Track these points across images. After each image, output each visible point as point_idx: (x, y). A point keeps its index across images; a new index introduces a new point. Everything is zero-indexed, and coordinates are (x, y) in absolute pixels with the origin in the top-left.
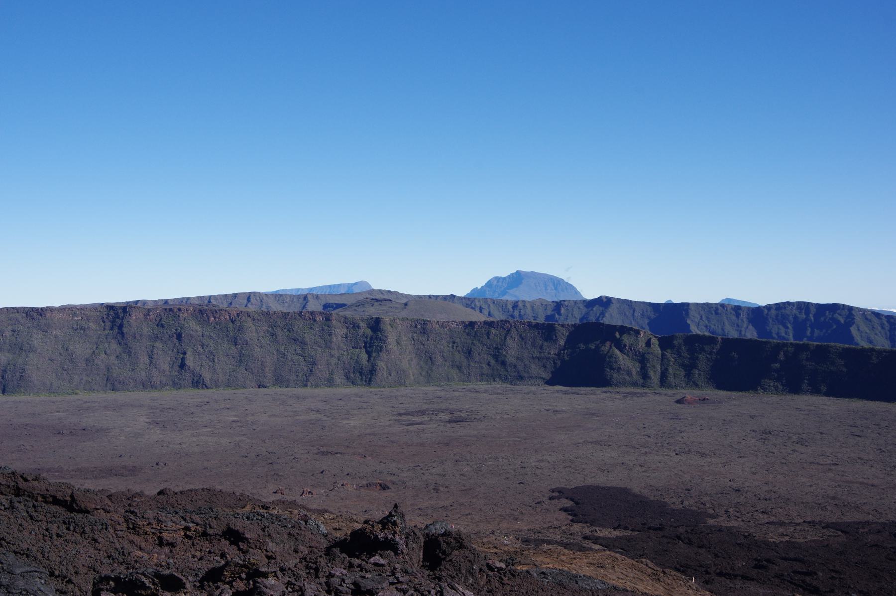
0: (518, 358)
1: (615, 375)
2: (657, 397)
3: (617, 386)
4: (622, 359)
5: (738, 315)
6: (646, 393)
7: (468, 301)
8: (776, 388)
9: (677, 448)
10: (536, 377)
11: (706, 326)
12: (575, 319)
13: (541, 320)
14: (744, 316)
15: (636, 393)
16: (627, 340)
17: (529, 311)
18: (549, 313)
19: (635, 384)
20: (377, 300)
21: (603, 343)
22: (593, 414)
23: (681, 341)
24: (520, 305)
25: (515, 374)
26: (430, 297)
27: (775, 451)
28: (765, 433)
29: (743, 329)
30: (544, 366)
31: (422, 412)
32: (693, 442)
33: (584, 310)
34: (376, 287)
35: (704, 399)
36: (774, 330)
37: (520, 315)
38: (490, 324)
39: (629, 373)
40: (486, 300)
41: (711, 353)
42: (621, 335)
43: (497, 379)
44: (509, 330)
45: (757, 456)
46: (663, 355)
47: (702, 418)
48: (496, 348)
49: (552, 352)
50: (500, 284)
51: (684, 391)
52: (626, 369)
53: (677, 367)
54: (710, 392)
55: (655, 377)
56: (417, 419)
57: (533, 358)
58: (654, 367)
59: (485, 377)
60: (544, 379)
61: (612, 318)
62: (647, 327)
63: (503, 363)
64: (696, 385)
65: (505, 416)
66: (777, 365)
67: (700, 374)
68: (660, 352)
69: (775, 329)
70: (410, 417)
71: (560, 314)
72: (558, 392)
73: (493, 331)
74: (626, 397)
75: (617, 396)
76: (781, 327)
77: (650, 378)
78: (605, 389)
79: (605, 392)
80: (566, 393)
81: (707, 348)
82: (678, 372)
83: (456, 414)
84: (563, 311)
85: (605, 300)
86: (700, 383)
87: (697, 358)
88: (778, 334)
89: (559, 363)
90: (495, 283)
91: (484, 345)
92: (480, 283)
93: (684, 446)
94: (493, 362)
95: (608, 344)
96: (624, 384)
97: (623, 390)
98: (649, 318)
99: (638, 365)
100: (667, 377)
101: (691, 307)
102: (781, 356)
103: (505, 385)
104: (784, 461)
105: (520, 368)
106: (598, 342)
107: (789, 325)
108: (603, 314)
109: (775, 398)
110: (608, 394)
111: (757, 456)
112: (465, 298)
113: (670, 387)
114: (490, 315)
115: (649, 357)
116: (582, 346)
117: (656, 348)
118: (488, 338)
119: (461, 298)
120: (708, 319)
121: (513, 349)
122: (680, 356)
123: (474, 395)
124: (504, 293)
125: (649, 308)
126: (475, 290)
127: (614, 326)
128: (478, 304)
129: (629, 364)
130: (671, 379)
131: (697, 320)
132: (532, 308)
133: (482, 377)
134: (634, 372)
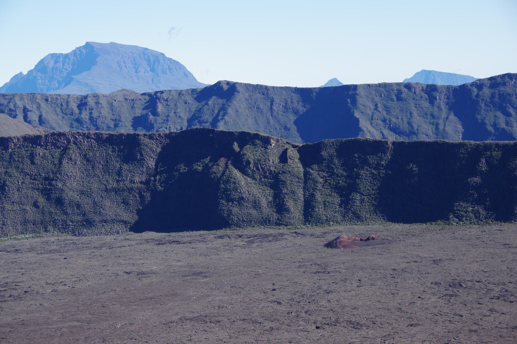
0: (82, 193)
1: (235, 210)
2: (299, 240)
3: (238, 226)
4: (245, 184)
5: (432, 100)
6: (282, 235)
8: (477, 215)
9: (319, 318)
10: (113, 221)
11: (384, 121)
12: (177, 124)
13: (126, 129)
14: (441, 100)
15: (267, 236)
16: (251, 153)
17: (105, 111)
18: (138, 112)
19: (265, 222)
21: (215, 160)
22: (199, 274)
23: (332, 151)
24: (91, 101)
25: (79, 218)
27: (464, 312)
28: (452, 285)
29: (441, 121)
30: (125, 203)
32: (343, 307)
33: (194, 105)
35: (368, 239)
36: (489, 120)
37: (91, 119)
38: (34, 140)
39: (256, 205)
40: (32, 97)
41: (377, 167)
42: (241, 147)
43: (50, 228)
44: (66, 149)
45: (436, 322)
46: (306, 174)
47: (362, 269)
48: (46, 179)
49: (137, 179)
50: (60, 65)
51: (340, 228)
52: (251, 199)
53: (328, 191)
54: (379, 227)
55: (295, 207)
57: (106, 190)
58: (293, 192)
59: (30, 226)
60: (125, 222)
61: (237, 119)
62: (294, 129)
63: (59, 202)
64: (358, 217)
65: (61, 288)
66: (477, 179)
67: (362, 201)
68: (302, 169)
69: (490, 117)
71: (155, 113)
72: (147, 241)
73: (40, 151)
74: (252, 242)
75: (239, 242)
76: (499, 114)
77: (288, 210)
78: (220, 232)
79: (221, 237)
80: (160, 243)
81: (372, 159)
82: (330, 199)
84: (160, 108)
85: (225, 87)
86: (363, 214)
87: (358, 175)
88: (494, 125)
89: (148, 196)
90: (51, 64)
91: (26, 174)
92: (26, 66)
93: (331, 314)
94: (42, 200)
95: (222, 161)
96: (249, 222)
97: (248, 231)
98: (296, 112)
99: (269, 191)
100: (313, 208)
101: (360, 91)
102: (483, 165)
103: (63, 237)
104: (474, 327)
105: (87, 208)
106: (207, 160)
107: (511, 111)
108: (223, 109)
109: (473, 230)
110: (226, 240)
111: (436, 322)
113: (319, 222)
114: (41, 121)
115: (287, 178)
116: (183, 168)
117: (295, 165)
118: (33, 163)
120: (387, 109)
121: (73, 179)
122: (332, 174)
123: (13, 256)
124: (68, 81)
125: (296, 97)
126: (18, 77)
127: (231, 134)
128: (20, 104)
129: (256, 192)
130: (320, 210)
131: (370, 112)
132: (111, 105)
133: (26, 226)
134: (264, 202)
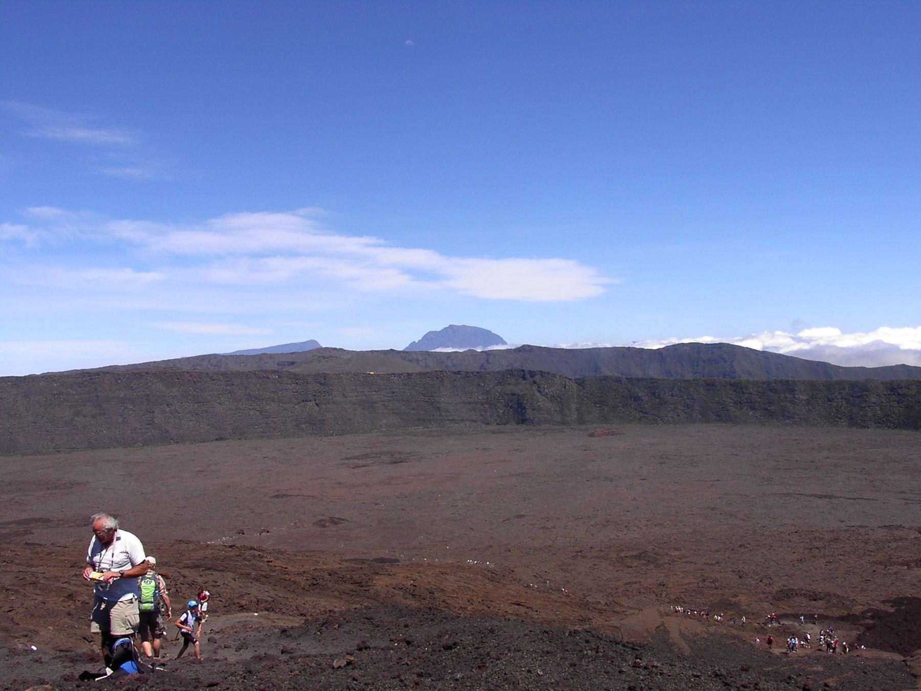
7: (404, 355)
20: (324, 358)
26: (372, 351)
31: (366, 456)
34: (324, 344)
56: (361, 462)
70: (357, 461)
83: (397, 456)
112: (403, 352)
119: (399, 352)
